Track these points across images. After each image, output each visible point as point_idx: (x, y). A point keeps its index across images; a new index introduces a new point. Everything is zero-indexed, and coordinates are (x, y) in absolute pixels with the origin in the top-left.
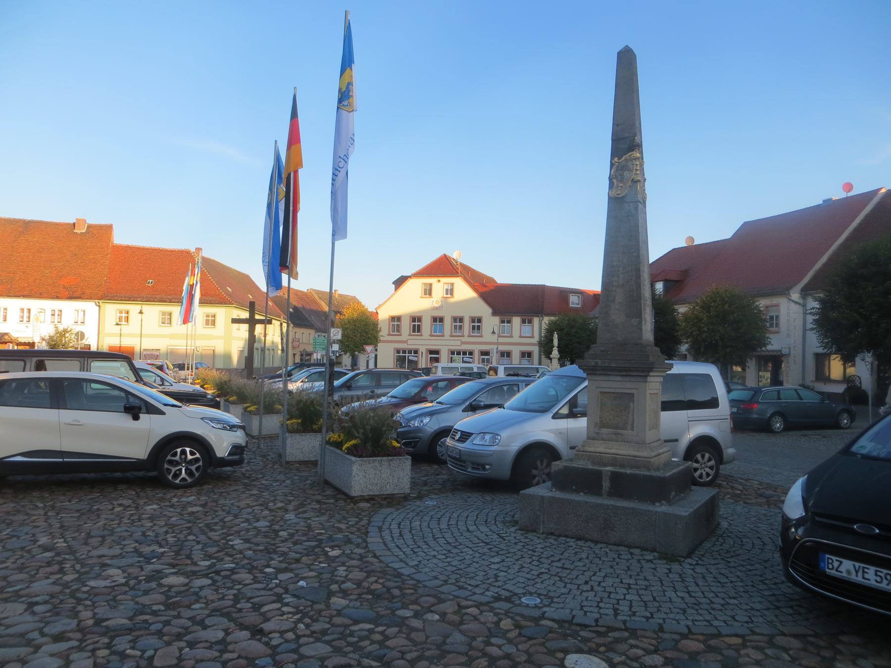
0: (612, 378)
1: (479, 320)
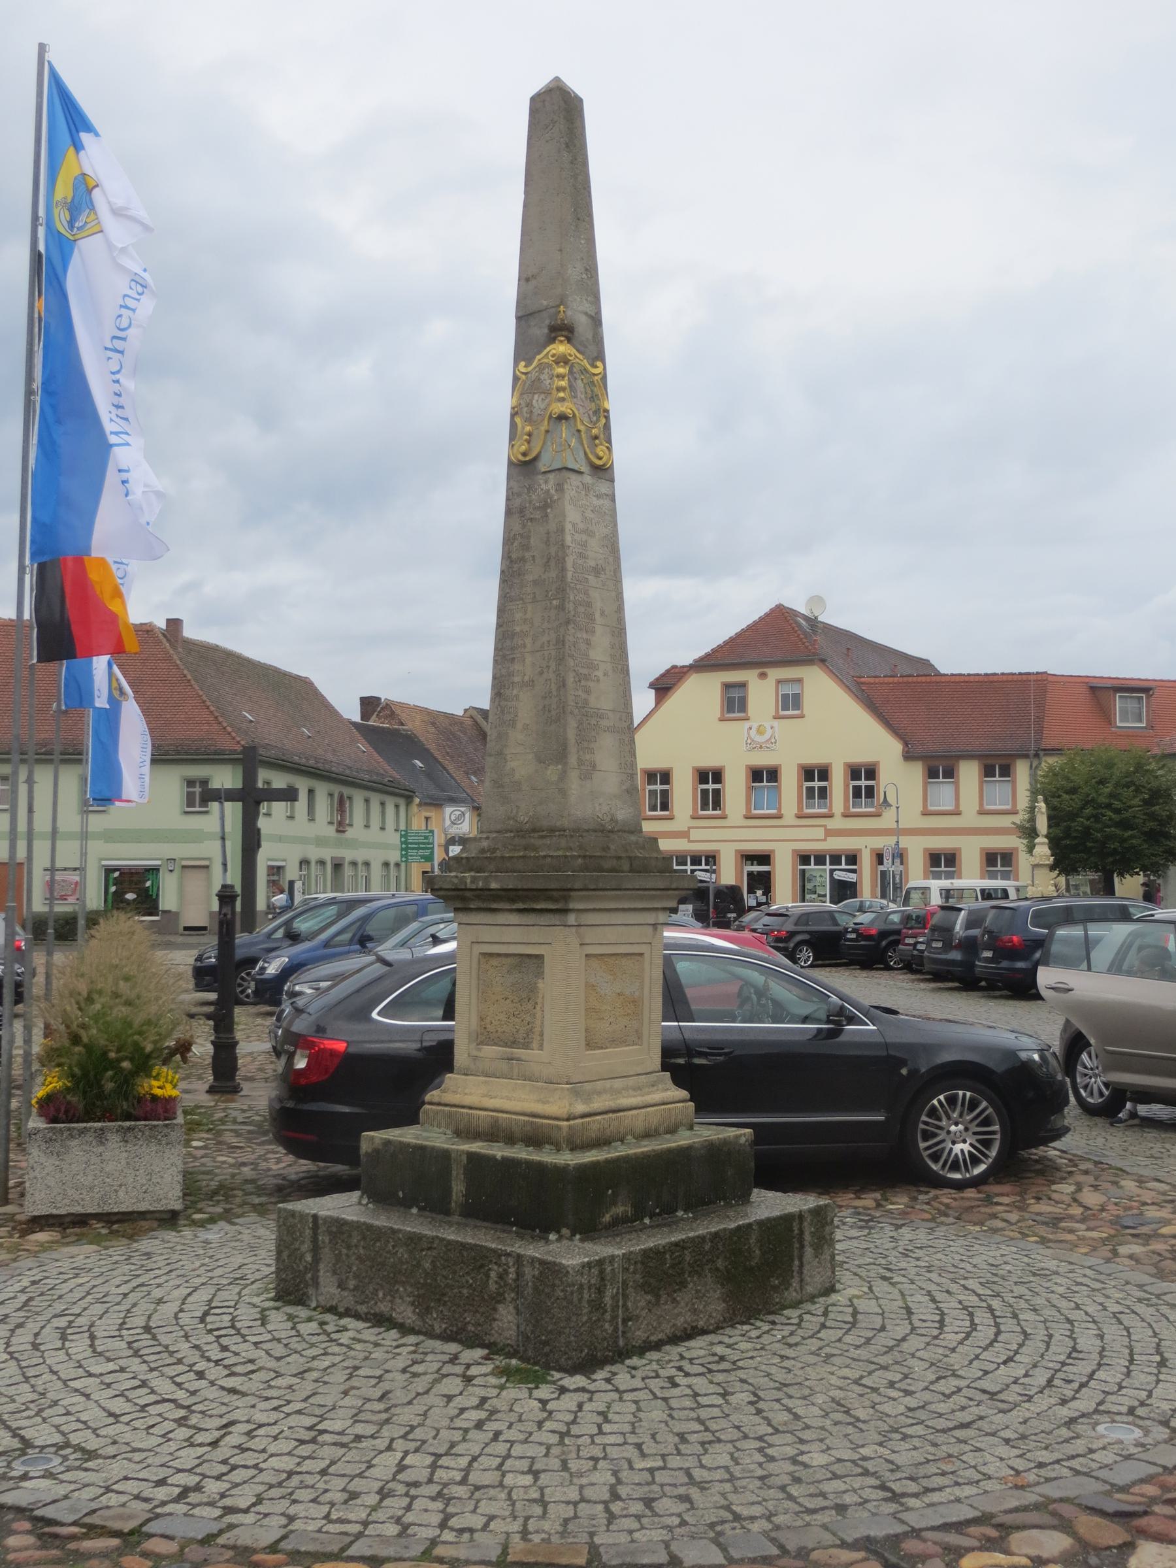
0: (501, 918)
1: (871, 773)
